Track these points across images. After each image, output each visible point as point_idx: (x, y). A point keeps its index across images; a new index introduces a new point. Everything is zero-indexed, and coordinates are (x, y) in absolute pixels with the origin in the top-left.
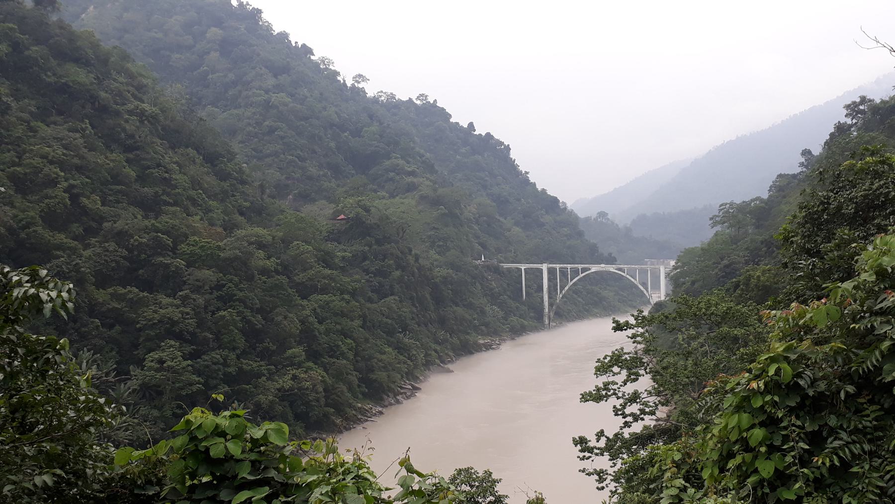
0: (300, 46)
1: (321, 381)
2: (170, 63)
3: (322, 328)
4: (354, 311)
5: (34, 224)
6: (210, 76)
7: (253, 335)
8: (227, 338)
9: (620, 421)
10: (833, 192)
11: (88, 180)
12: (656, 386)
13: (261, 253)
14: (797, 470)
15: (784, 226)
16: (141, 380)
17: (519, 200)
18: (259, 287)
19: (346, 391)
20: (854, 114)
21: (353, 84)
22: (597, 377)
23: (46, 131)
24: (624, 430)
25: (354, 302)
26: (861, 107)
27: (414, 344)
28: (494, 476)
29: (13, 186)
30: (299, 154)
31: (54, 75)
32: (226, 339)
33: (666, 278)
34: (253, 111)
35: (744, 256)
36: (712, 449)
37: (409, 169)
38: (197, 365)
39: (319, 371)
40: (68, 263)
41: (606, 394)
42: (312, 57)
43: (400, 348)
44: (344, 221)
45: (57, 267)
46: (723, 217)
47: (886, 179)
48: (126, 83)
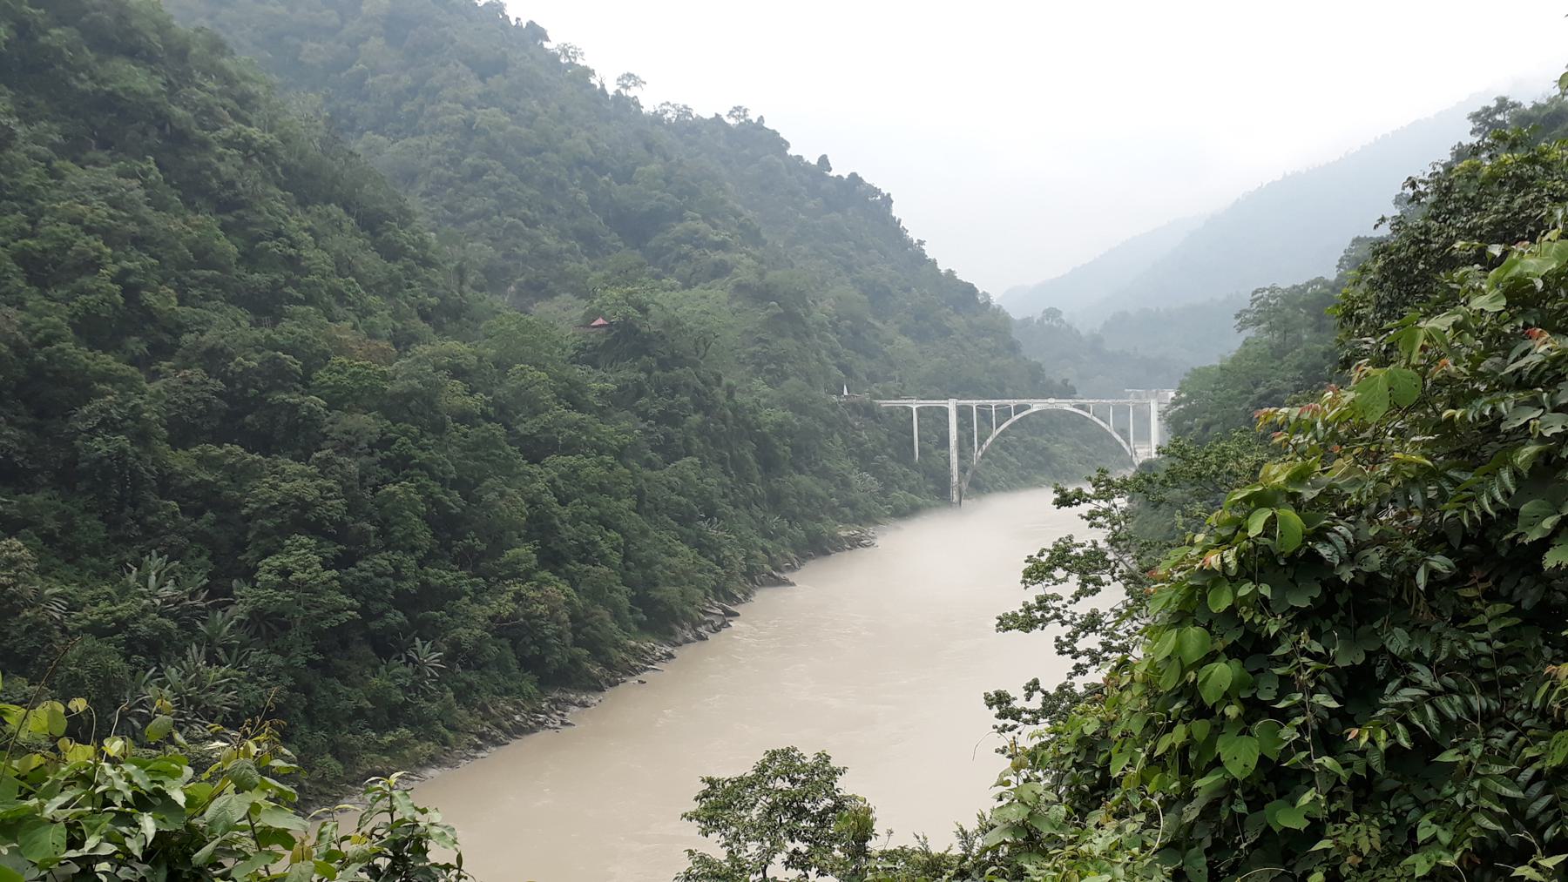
0: (524, 26)
1: (566, 603)
2: (300, 58)
3: (566, 512)
4: (620, 484)
5: (59, 338)
6: (370, 80)
7: (444, 524)
8: (400, 532)
9: (1068, 663)
10: (1437, 221)
11: (153, 261)
12: (1130, 602)
13: (458, 386)
14: (1309, 758)
15: (1345, 290)
16: (252, 603)
17: (908, 290)
18: (455, 444)
19: (608, 618)
20: (1487, 129)
21: (618, 92)
22: (1026, 588)
23: (78, 176)
24: (1075, 679)
25: (621, 468)
26: (1499, 117)
27: (727, 538)
28: (834, 763)
29: (23, 272)
30: (525, 214)
31: (92, 78)
32: (398, 532)
33: (1159, 420)
34: (446, 138)
35: (1294, 379)
36: (1133, 712)
37: (716, 238)
38: (349, 579)
39: (561, 586)
40: (120, 405)
41: (1042, 616)
42: (546, 45)
43: (703, 546)
44: (604, 330)
45: (102, 411)
46: (1259, 311)
47: (1539, 191)
48: (219, 91)
